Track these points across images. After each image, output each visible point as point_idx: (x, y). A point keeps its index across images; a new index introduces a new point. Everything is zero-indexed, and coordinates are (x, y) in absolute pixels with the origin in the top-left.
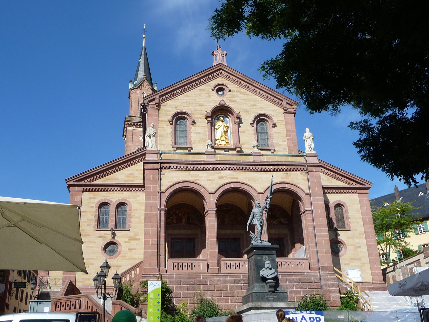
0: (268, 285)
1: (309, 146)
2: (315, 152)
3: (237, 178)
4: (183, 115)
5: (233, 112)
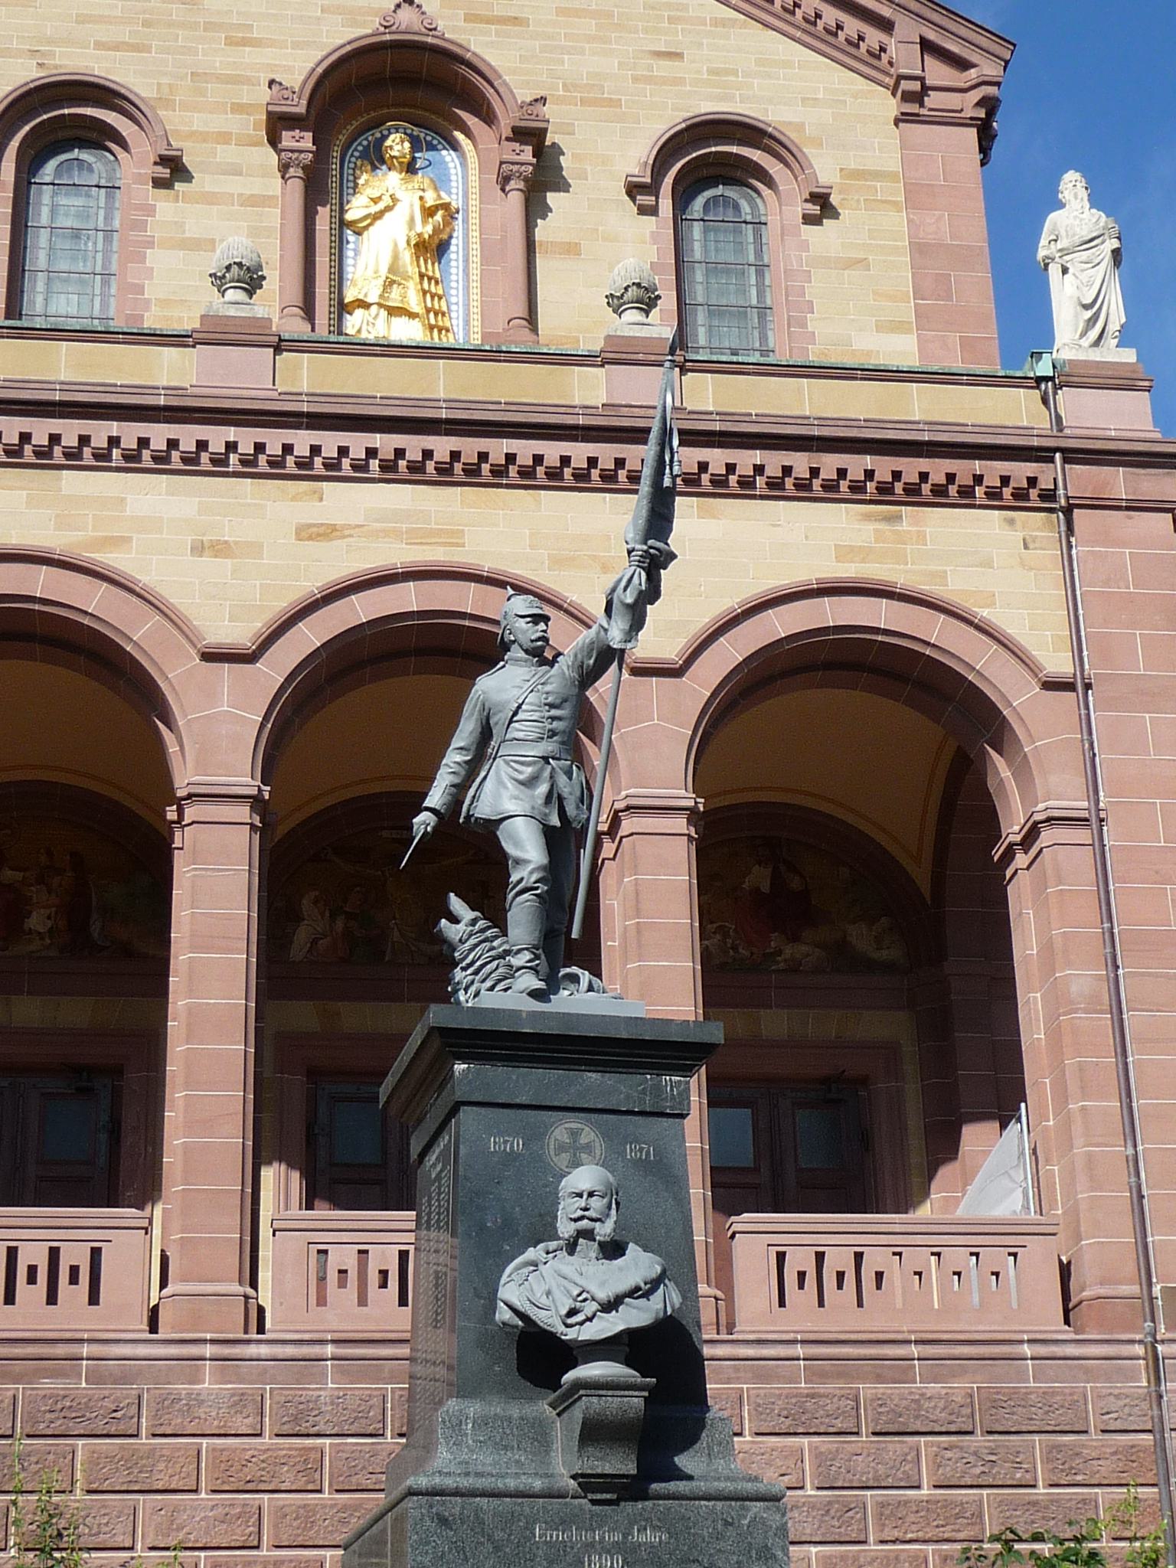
0: (577, 1413)
1: (1086, 307)
2: (1129, 356)
3: (453, 536)
4: (89, 111)
5: (489, 92)
